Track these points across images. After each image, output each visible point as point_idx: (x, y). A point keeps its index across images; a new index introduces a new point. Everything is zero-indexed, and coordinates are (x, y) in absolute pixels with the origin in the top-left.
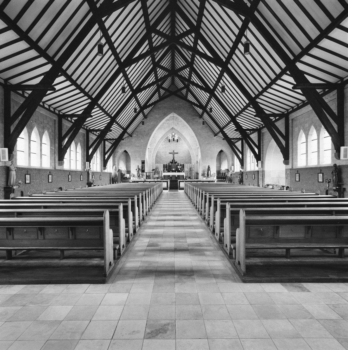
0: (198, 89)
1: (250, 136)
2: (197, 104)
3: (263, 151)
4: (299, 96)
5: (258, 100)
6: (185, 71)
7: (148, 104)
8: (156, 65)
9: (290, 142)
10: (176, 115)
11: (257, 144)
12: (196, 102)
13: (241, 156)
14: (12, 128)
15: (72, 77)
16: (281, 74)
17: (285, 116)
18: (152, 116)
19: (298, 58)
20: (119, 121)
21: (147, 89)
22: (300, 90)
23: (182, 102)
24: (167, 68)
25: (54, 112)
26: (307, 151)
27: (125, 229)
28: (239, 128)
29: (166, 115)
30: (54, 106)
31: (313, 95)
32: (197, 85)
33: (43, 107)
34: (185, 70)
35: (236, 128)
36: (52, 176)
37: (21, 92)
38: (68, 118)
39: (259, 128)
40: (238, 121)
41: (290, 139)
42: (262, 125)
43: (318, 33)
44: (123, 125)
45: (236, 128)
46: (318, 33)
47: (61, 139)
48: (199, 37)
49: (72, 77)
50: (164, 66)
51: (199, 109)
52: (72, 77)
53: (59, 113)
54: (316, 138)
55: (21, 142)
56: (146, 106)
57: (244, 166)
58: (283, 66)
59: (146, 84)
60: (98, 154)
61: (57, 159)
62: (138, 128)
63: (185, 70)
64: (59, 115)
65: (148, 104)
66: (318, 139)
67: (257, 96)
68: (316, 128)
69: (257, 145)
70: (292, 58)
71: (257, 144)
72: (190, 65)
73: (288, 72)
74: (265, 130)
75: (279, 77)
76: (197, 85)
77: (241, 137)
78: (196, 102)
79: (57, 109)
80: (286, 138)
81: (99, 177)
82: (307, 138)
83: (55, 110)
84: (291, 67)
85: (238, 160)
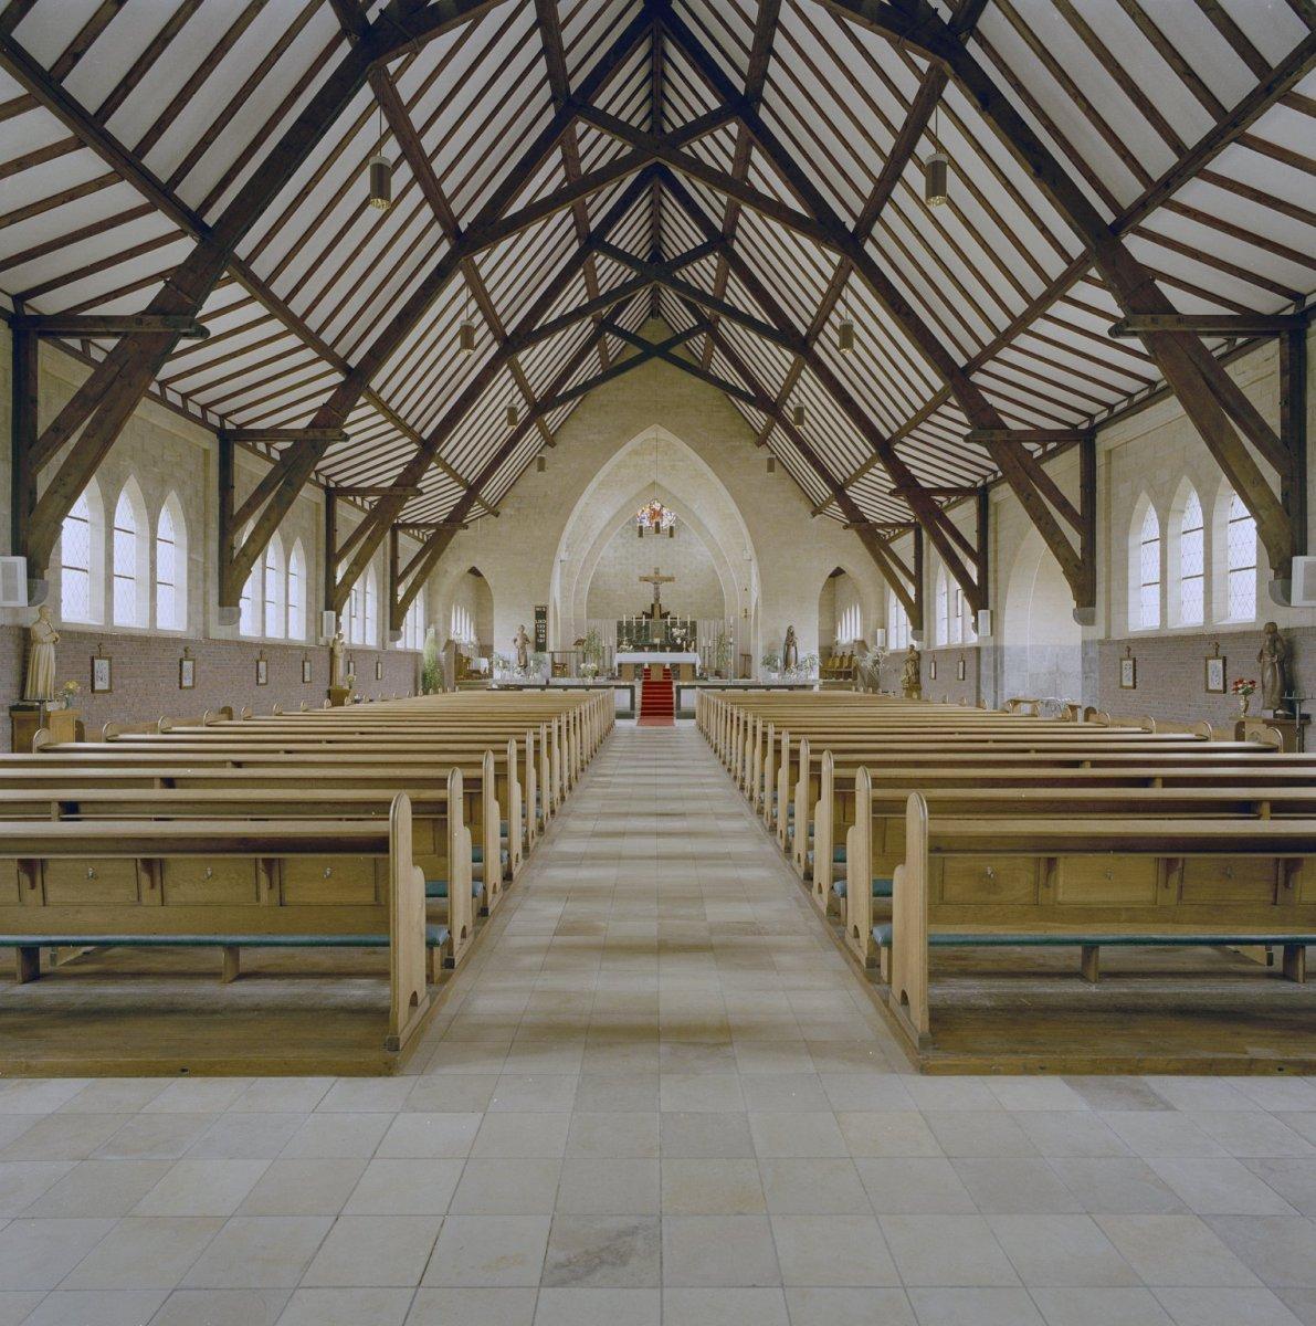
7: (537, 327)
8: (593, 241)
10: (665, 435)
14: (43, 481)
16: (1067, 279)
17: (1084, 438)
19: (1129, 218)
28: (905, 483)
30: (203, 398)
31: (1190, 361)
33: (162, 400)
38: (255, 446)
46: (1208, 123)
47: (228, 522)
53: (222, 423)
55: (76, 537)
58: (1076, 247)
59: (552, 314)
64: (327, 489)
65: (537, 327)
70: (1108, 217)
73: (1093, 272)
74: (1004, 495)
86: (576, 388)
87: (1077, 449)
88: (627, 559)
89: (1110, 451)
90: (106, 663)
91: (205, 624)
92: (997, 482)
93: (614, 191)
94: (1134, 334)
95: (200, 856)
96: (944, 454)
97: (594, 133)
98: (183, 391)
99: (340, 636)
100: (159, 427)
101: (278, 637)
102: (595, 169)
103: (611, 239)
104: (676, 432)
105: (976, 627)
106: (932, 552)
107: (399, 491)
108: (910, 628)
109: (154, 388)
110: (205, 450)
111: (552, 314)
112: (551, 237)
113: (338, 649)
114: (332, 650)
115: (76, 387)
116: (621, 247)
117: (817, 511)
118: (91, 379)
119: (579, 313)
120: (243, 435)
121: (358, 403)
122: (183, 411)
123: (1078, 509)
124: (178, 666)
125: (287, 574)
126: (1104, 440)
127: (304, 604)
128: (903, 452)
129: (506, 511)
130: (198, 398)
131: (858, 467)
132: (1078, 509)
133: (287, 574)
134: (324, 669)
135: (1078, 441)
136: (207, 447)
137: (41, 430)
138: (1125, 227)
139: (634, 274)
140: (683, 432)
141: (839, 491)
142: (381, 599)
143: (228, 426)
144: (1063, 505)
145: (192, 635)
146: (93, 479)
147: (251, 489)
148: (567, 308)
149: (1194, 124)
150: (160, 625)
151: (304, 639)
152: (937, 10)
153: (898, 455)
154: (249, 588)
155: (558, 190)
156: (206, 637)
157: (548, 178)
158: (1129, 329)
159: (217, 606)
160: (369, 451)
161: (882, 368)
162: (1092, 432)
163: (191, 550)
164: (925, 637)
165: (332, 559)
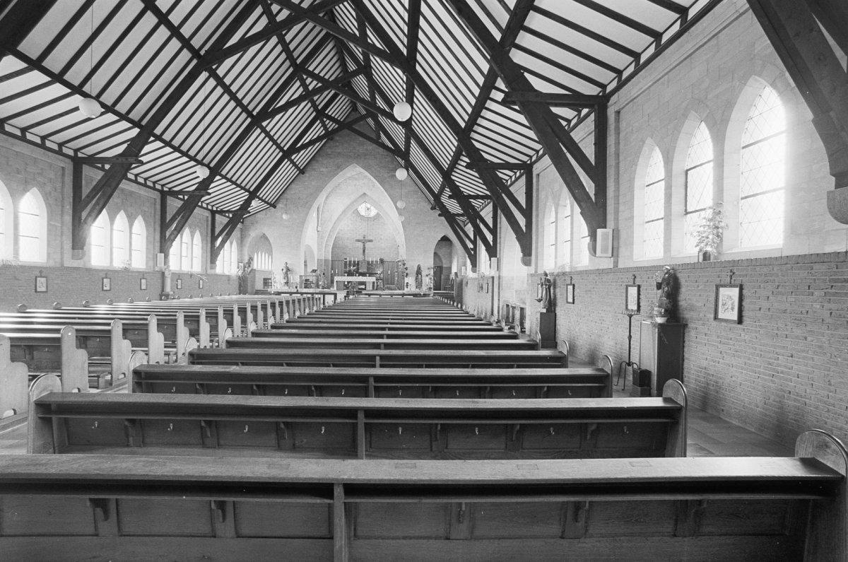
0: (385, 63)
2: (385, 51)
3: (500, 238)
6: (341, 9)
7: (299, 145)
8: (321, 114)
10: (359, 169)
11: (524, 205)
14: (168, 234)
18: (314, 170)
20: (272, 129)
21: (310, 148)
23: (370, 146)
24: (339, 119)
25: (154, 188)
29: (339, 168)
30: (154, 179)
33: (201, 207)
34: (340, 7)
36: (722, 286)
37: (100, 165)
38: (103, 166)
44: (296, 159)
47: (164, 226)
50: (336, 117)
53: (162, 188)
55: (174, 249)
56: (294, 149)
59: (306, 139)
60: (195, 239)
61: (209, 262)
62: (288, 191)
63: (340, 7)
64: (162, 192)
65: (299, 145)
69: (594, 164)
71: (524, 205)
72: (366, 69)
79: (141, 175)
83: (63, 148)
88: (353, 231)
90: (43, 280)
91: (62, 259)
97: (331, 123)
98: (43, 134)
99: (168, 266)
100: (20, 153)
101: (105, 265)
103: (309, 67)
104: (364, 168)
105: (593, 249)
107: (197, 193)
109: (130, 176)
110: (63, 168)
111: (306, 139)
113: (166, 273)
114: (163, 273)
115: (177, 207)
118: (103, 176)
119: (319, 139)
120: (172, 193)
121: (150, 140)
122: (145, 185)
124: (34, 281)
125: (131, 233)
127: (145, 250)
129: (280, 206)
130: (56, 138)
133: (131, 233)
134: (207, 280)
136: (63, 166)
137: (84, 197)
140: (367, 168)
142: (205, 248)
143: (165, 189)
145: (51, 264)
146: (104, 211)
147: (172, 212)
148: (295, 111)
150: (183, 269)
151: (145, 267)
154: (220, 258)
155: (301, 96)
156: (62, 266)
157: (295, 90)
159: (71, 250)
160: (224, 194)
163: (50, 219)
165: (214, 238)
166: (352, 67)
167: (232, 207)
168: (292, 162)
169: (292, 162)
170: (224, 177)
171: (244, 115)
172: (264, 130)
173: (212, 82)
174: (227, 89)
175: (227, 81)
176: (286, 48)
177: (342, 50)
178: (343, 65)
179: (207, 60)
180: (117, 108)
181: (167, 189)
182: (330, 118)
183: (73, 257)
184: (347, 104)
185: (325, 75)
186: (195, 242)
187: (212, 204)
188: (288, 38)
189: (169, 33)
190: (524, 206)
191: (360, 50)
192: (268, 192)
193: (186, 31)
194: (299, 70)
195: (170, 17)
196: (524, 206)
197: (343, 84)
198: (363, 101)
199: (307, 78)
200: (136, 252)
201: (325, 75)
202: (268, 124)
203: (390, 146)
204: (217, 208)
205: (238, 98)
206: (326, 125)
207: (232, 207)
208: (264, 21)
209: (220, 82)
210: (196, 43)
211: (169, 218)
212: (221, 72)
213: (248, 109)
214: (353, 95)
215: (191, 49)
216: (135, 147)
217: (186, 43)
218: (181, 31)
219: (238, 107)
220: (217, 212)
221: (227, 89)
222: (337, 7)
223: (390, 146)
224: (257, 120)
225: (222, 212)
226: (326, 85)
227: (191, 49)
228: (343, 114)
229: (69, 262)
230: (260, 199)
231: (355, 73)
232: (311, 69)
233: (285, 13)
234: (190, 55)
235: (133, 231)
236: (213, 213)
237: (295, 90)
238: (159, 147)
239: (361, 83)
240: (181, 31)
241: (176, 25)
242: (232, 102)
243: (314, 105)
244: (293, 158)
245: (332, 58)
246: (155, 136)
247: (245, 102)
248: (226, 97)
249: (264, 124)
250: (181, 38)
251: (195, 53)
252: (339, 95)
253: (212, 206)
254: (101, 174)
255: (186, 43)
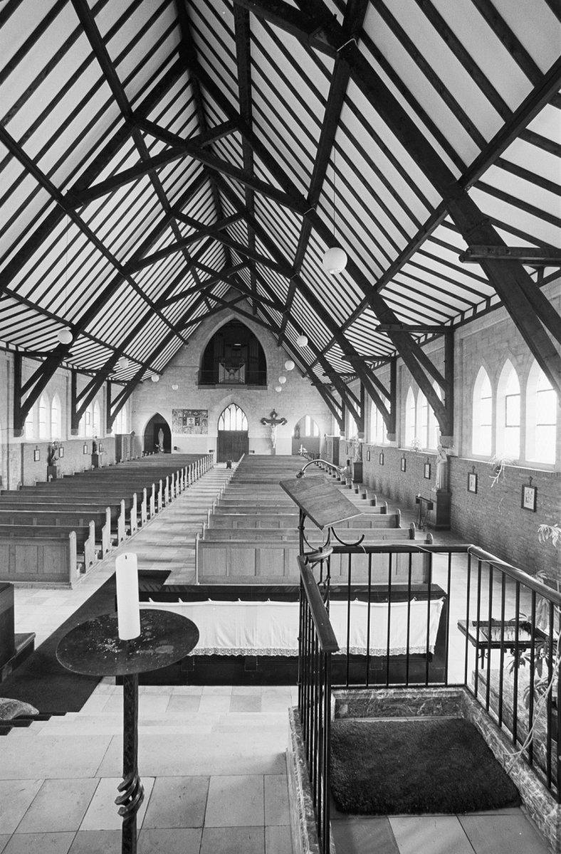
1: (423, 348)
4: (473, 282)
5: (383, 292)
8: (193, 263)
9: (365, 409)
12: (268, 297)
13: (358, 410)
15: (97, 235)
16: (431, 225)
17: (447, 332)
19: (472, 173)
20: (147, 290)
22: (478, 265)
26: (523, 418)
27: (143, 613)
28: (350, 353)
31: (515, 277)
32: (268, 191)
35: (344, 355)
39: (393, 355)
40: (347, 337)
41: (398, 399)
42: (488, 299)
43: (500, 123)
44: (168, 316)
45: (344, 355)
46: (500, 123)
48: (252, 145)
49: (38, 165)
51: (283, 279)
52: (38, 165)
53: (17, 348)
54: (490, 394)
56: (163, 302)
57: (365, 430)
58: (436, 199)
65: (169, 297)
66: (523, 394)
67: (381, 283)
68: (490, 373)
70: (457, 174)
72: (247, 212)
73: (448, 219)
74: (400, 362)
75: (425, 231)
76: (268, 191)
77: (395, 351)
78: (268, 297)
80: (448, 384)
81: (520, 491)
82: (495, 388)
84: (455, 203)
85: (380, 416)
86: (197, 319)
87: (443, 338)
89: (462, 340)
92: (398, 356)
93: (197, 245)
94: (474, 260)
95: (398, 373)
96: (367, 336)
102: (187, 236)
106: (406, 376)
108: (386, 432)
109: (64, 364)
112: (176, 260)
116: (206, 265)
117: (303, 376)
119: (191, 291)
123: (389, 392)
126: (459, 335)
128: (348, 334)
131: (344, 321)
132: (389, 392)
133: (51, 409)
135: (443, 333)
138: (469, 180)
139: (210, 276)
141: (338, 333)
144: (355, 399)
149: (403, 244)
152: (336, 15)
153: (346, 336)
158: (472, 256)
160: (125, 368)
161: (328, 289)
162: (453, 328)
164: (397, 440)
166: (230, 210)
167: (86, 365)
168: (161, 316)
169: (161, 316)
170: (87, 335)
171: (111, 266)
172: (132, 282)
173: (75, 229)
174: (99, 245)
175: (100, 236)
176: (159, 189)
177: (219, 188)
178: (201, 112)
179: (71, 201)
180: (19, 292)
181: (23, 350)
182: (214, 297)
183: (107, 433)
184: (221, 258)
185: (204, 221)
186: (95, 410)
187: (72, 363)
188: (161, 177)
189: (22, 168)
190: (487, 279)
191: (244, 186)
192: (158, 363)
193: (44, 166)
194: (173, 213)
195: (24, 148)
196: (487, 279)
197: (218, 231)
198: (239, 247)
199: (180, 223)
200: (43, 424)
201: (204, 221)
202: (138, 277)
203: (268, 322)
204: (17, 346)
205: (111, 254)
206: (198, 276)
207: (86, 365)
208: (135, 157)
209: (84, 228)
210: (56, 180)
211: (112, 400)
212: (85, 217)
213: (102, 251)
214: (228, 243)
215: (50, 188)
216: (113, 361)
217: (44, 181)
218: (51, 180)
219: (104, 257)
220: (112, 382)
221: (99, 245)
222: (217, 142)
223: (268, 322)
224: (126, 272)
225: (84, 371)
226: (201, 230)
227: (50, 188)
228: (217, 262)
229: (72, 437)
230: (127, 357)
231: (234, 218)
232: (185, 212)
233: (161, 145)
234: (49, 196)
235: (53, 407)
236: (74, 372)
237: (167, 238)
238: (12, 304)
239: (240, 231)
240: (51, 180)
241: (32, 158)
242: (105, 258)
243: (186, 254)
244: (162, 312)
245: (209, 207)
246: (8, 291)
247: (112, 251)
248: (91, 246)
249: (133, 276)
250: (38, 174)
251: (55, 193)
252: (213, 240)
253: (73, 365)
254: (41, 363)
255: (44, 181)
